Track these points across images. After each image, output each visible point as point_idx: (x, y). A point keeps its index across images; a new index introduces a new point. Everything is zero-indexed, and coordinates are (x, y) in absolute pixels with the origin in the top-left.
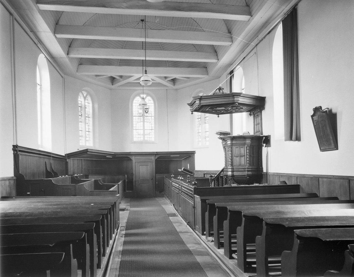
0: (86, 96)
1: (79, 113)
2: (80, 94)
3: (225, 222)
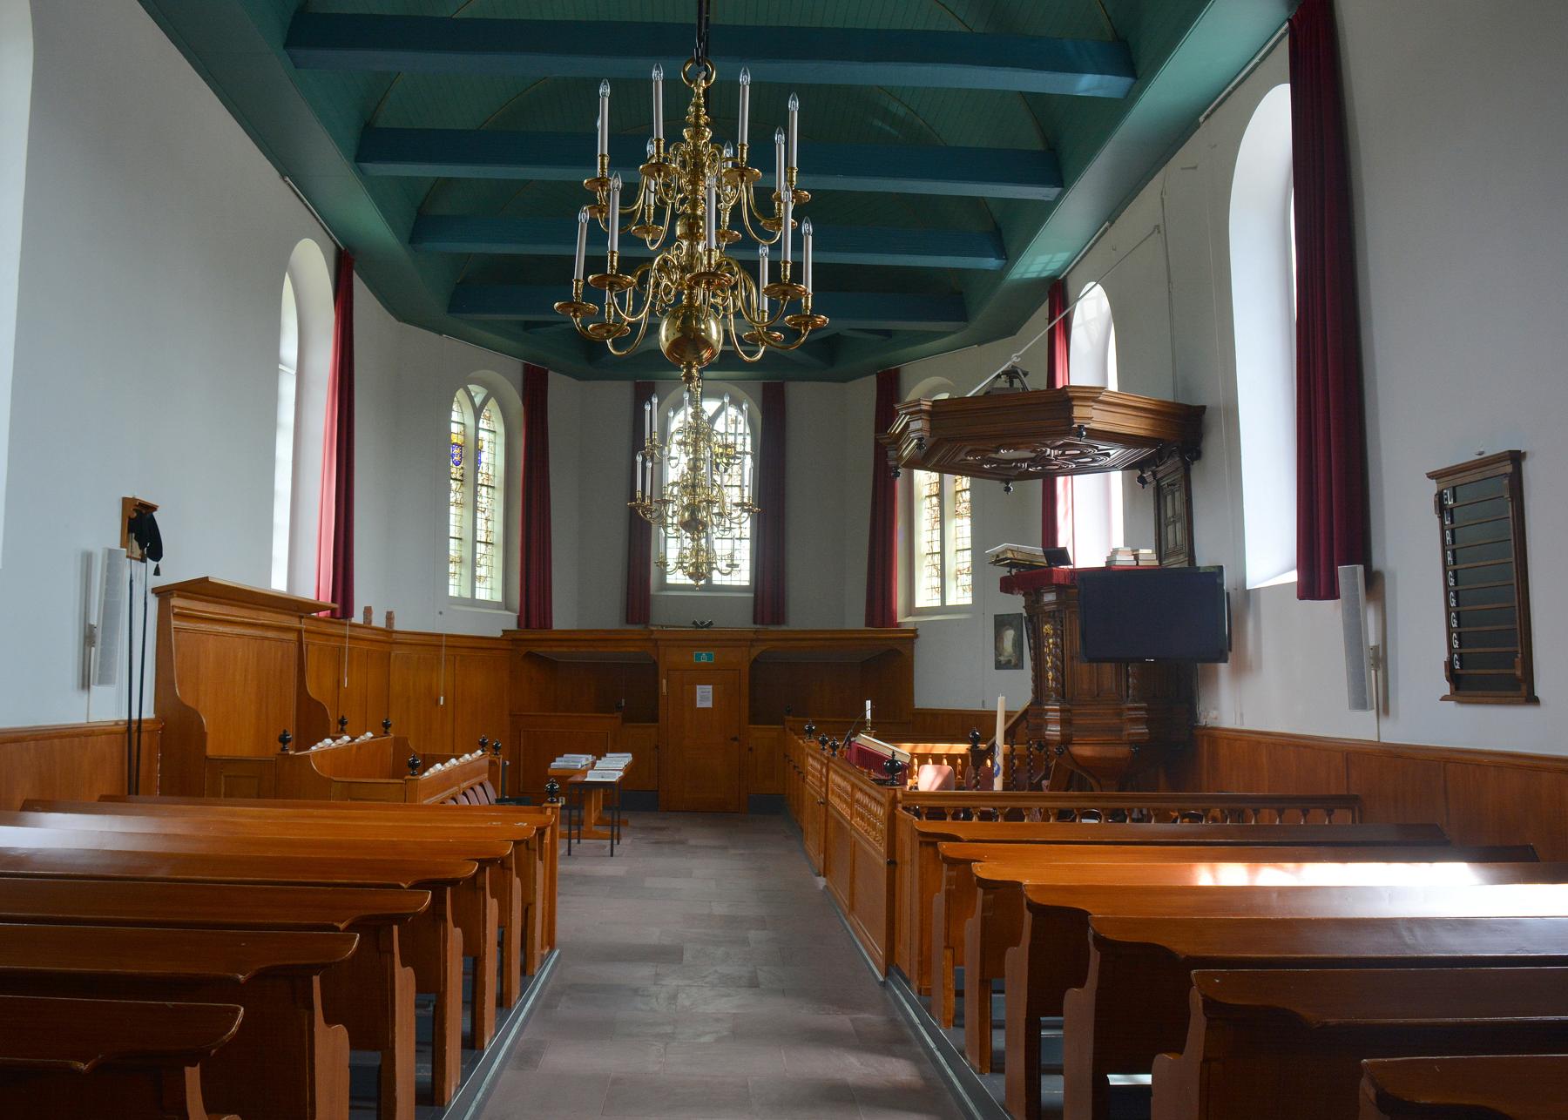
0: (485, 402)
1: (453, 470)
2: (460, 394)
3: (1011, 952)
